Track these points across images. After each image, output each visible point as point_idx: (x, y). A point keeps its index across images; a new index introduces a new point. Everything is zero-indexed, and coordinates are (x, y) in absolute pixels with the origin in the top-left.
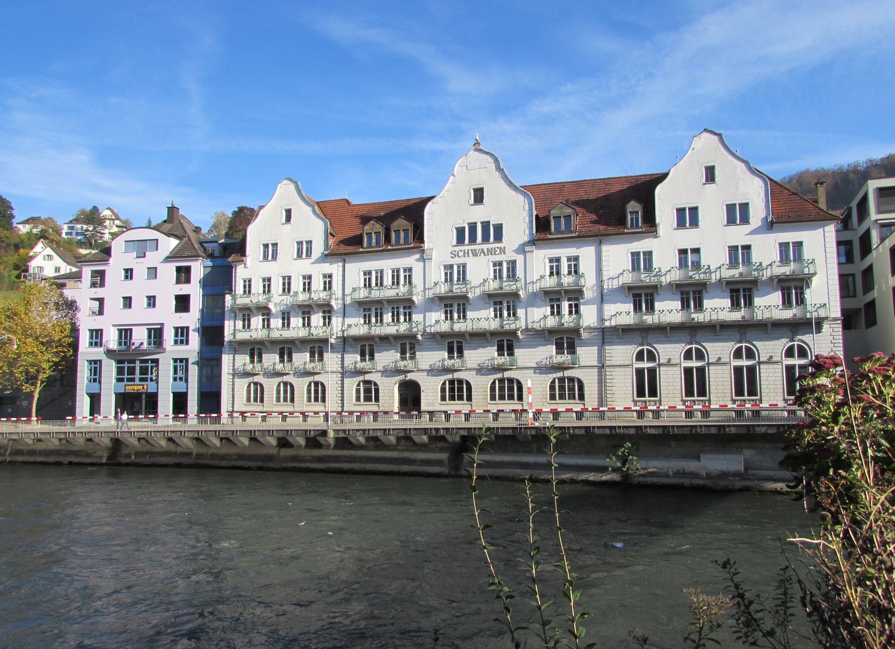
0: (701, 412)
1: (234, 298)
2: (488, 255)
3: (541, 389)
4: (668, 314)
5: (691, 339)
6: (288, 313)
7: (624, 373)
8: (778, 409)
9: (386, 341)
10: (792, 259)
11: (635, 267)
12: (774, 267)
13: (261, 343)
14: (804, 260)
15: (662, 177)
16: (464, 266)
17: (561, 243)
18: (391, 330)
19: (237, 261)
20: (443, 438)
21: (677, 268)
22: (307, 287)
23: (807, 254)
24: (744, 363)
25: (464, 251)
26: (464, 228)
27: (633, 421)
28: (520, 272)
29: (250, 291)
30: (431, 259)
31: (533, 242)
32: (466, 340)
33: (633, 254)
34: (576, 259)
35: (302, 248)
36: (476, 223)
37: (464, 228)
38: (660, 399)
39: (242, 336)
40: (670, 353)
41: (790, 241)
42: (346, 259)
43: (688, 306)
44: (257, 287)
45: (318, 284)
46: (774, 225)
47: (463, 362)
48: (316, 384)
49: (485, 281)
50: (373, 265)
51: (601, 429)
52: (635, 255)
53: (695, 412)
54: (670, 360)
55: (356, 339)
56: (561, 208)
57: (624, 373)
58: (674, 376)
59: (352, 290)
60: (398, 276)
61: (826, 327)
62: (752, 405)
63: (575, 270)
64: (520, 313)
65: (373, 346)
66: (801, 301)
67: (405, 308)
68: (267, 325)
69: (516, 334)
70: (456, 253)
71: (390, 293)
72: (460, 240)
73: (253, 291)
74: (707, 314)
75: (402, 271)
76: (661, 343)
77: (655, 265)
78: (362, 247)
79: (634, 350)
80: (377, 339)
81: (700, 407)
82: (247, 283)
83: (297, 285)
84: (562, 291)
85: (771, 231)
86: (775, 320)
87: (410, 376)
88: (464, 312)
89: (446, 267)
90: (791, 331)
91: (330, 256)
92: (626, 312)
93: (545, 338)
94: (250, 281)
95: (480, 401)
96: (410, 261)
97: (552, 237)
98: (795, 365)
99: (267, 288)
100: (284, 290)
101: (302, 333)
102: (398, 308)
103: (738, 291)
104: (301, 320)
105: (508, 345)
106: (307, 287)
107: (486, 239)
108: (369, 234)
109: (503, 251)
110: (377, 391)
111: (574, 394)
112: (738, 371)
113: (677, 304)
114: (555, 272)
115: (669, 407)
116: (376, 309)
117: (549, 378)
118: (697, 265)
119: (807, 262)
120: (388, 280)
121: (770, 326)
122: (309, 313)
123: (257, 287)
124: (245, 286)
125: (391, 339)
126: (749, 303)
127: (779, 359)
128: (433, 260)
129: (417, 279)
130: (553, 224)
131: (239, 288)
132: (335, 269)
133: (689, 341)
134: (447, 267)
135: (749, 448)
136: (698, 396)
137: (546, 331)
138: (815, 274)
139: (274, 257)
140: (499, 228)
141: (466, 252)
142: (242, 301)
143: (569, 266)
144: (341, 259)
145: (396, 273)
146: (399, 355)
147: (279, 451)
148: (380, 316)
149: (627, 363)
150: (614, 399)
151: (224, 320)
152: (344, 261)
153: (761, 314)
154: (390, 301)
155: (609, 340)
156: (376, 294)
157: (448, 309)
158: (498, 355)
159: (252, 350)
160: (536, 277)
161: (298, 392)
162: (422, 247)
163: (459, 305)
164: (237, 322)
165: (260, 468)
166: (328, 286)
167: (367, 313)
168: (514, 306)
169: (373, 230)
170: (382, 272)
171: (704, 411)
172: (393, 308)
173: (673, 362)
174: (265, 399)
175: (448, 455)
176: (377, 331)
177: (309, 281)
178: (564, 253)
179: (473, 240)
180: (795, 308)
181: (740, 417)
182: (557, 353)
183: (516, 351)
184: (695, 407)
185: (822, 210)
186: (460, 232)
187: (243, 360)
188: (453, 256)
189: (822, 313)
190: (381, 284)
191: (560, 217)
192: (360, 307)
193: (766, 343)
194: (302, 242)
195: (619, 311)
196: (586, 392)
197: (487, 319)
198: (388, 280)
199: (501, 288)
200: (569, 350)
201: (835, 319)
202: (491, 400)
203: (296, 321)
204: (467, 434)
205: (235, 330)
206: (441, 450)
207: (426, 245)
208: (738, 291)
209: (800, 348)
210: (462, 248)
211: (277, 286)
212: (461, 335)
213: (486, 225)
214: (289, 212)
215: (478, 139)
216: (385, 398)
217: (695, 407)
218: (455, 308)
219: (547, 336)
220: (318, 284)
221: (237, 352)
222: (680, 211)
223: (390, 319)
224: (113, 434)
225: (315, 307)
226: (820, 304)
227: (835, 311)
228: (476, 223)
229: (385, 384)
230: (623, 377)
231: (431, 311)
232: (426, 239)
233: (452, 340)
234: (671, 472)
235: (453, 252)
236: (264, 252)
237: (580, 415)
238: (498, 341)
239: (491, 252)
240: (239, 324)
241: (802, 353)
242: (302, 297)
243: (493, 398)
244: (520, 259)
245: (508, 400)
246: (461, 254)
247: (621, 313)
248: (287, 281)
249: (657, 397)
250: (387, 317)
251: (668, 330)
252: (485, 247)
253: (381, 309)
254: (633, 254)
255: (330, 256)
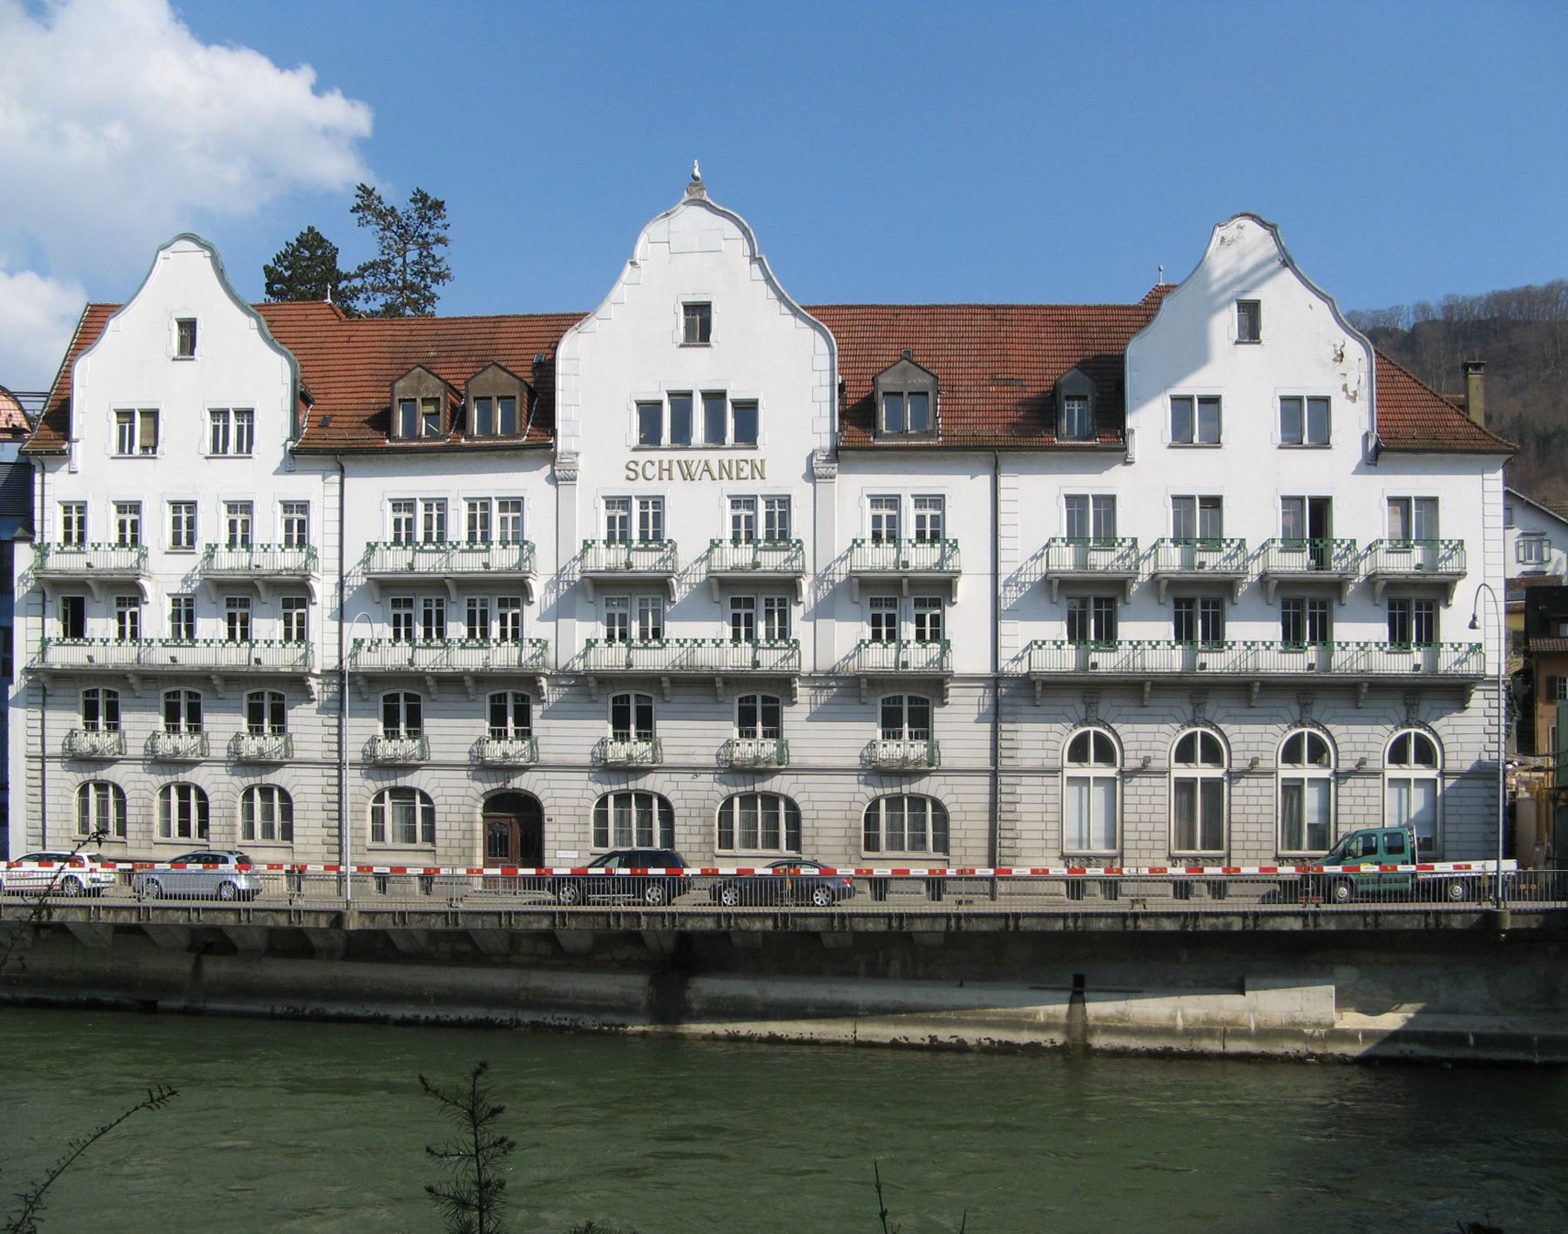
0: (1067, 882)
1: (43, 550)
2: (721, 478)
3: (846, 824)
4: (1149, 654)
5: (1408, 713)
6: (189, 602)
7: (1042, 790)
8: (1241, 878)
9: (454, 685)
10: (1091, 535)
11: (1075, 535)
12: (1380, 553)
13: (118, 677)
14: (1335, 541)
15: (574, 319)
16: (659, 502)
17: (930, 458)
18: (469, 660)
19: (48, 453)
20: (635, 938)
21: (1063, 540)
22: (240, 536)
23: (1447, 529)
24: (1201, 771)
25: (660, 462)
26: (659, 404)
27: (1058, 904)
28: (800, 526)
29: (82, 538)
30: (574, 479)
31: (837, 454)
32: (429, 693)
33: (1070, 499)
34: (938, 501)
35: (132, 429)
36: (689, 394)
37: (659, 404)
38: (1229, 855)
39: (66, 656)
40: (1253, 746)
41: (1090, 492)
42: (344, 465)
43: (1190, 636)
44: (103, 526)
45: (269, 526)
46: (1382, 455)
47: (533, 745)
48: (184, 790)
49: (714, 544)
50: (419, 485)
51: (1153, 920)
52: (1075, 503)
53: (1195, 884)
54: (1147, 760)
55: (373, 680)
56: (904, 371)
57: (1042, 790)
58: (1368, 801)
59: (708, 546)
60: (486, 520)
61: (1477, 699)
62: (1188, 870)
63: (932, 533)
64: (797, 632)
65: (418, 698)
66: (1429, 637)
67: (503, 603)
68: (130, 631)
69: (536, 682)
70: (639, 469)
71: (468, 563)
72: (650, 435)
73: (91, 536)
74: (1124, 650)
75: (495, 505)
76: (1235, 720)
77: (1121, 531)
78: (390, 436)
79: (1063, 735)
80: (430, 682)
81: (1101, 871)
82: (435, 513)
83: (212, 526)
84: (905, 581)
85: (1373, 467)
86: (1377, 677)
87: (521, 782)
88: (440, 622)
89: (611, 502)
90: (1299, 703)
91: (301, 454)
92: (714, 641)
93: (467, 694)
94: (82, 508)
95: (695, 848)
96: (528, 482)
97: (878, 443)
98: (1196, 779)
99: (130, 536)
100: (176, 540)
101: (234, 657)
102: (484, 602)
103: (1190, 603)
104: (114, 624)
105: (638, 709)
106: (240, 536)
107: (715, 435)
108: (408, 403)
109: (758, 471)
110: (429, 814)
111: (776, 836)
112: (1185, 787)
113: (1166, 630)
114: (886, 532)
115: (1034, 871)
116: (427, 602)
117: (482, 788)
118: (1214, 540)
119: (1447, 547)
120: (458, 528)
121: (1365, 690)
122: (245, 603)
123: (103, 526)
124: (68, 523)
125: (469, 682)
126: (1322, 635)
127: (1164, 764)
128: (577, 482)
129: (537, 525)
130: (400, 417)
131: (51, 525)
132: (314, 487)
133: (1190, 718)
134: (614, 502)
135: (1347, 963)
136: (1204, 848)
137: (590, 679)
138: (1461, 575)
139: (151, 448)
140: (747, 411)
141: (665, 466)
142: (64, 563)
143: (920, 520)
144: (333, 465)
145: (479, 510)
146: (487, 724)
147: (198, 966)
148: (436, 624)
149: (1049, 764)
150: (1016, 852)
151: (13, 615)
152: (342, 470)
153: (1343, 661)
154: (467, 584)
155: (1009, 709)
156: (428, 563)
157: (743, 612)
158: (741, 735)
159: (391, 700)
160: (841, 545)
161: (136, 811)
162: (550, 446)
163: (769, 602)
164: (47, 620)
165: (296, 1018)
166: (298, 533)
167: (403, 612)
168: (440, 614)
169: (418, 392)
170: (442, 504)
171: (1073, 882)
172: (471, 603)
173: (1154, 764)
174: (129, 827)
175: (648, 978)
176: (427, 659)
177: (244, 516)
178: (907, 484)
179: (682, 434)
180: (296, 642)
181: (807, 886)
182: (886, 736)
183: (427, 722)
184: (1089, 871)
185: (1474, 424)
186: (649, 412)
187: (65, 722)
188: (632, 475)
189: (1472, 667)
190: (441, 538)
191: (490, 398)
192: (382, 596)
193: (1353, 728)
194: (226, 413)
195: (1040, 638)
196: (952, 834)
197: (718, 643)
198: (458, 528)
199: (756, 565)
200: (886, 730)
201: (1495, 681)
202: (867, 848)
203: (211, 627)
204: (1178, 929)
205: (45, 642)
206: (626, 967)
207: (562, 443)
208: (1190, 603)
209: (1422, 743)
210: (655, 456)
211: (157, 528)
212: (652, 680)
213: (714, 398)
214: (188, 328)
215: (697, 173)
216: (450, 835)
217: (1089, 871)
218: (761, 608)
219: (594, 691)
220: (269, 526)
221: (49, 700)
222: (1291, 405)
223: (463, 630)
224: (495, 919)
225: (94, 588)
226: (1470, 644)
227: (1496, 660)
228: (689, 394)
229: (450, 800)
230: (1038, 799)
231: (572, 616)
232: (559, 425)
233: (897, 694)
234: (1180, 1022)
235: (632, 466)
236: (122, 430)
237: (936, 885)
238: (741, 700)
239: (726, 471)
240: (55, 627)
241: (1426, 755)
242: (230, 562)
243: (726, 841)
244: (801, 497)
245: (763, 847)
246: (652, 471)
247: (1044, 642)
248: (75, 516)
249: (1222, 849)
250: (457, 629)
251: (1148, 689)
252: (714, 457)
253: (440, 602)
254: (1070, 499)
255: (301, 454)
